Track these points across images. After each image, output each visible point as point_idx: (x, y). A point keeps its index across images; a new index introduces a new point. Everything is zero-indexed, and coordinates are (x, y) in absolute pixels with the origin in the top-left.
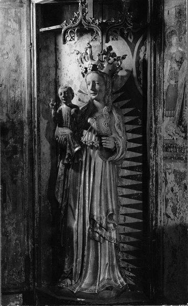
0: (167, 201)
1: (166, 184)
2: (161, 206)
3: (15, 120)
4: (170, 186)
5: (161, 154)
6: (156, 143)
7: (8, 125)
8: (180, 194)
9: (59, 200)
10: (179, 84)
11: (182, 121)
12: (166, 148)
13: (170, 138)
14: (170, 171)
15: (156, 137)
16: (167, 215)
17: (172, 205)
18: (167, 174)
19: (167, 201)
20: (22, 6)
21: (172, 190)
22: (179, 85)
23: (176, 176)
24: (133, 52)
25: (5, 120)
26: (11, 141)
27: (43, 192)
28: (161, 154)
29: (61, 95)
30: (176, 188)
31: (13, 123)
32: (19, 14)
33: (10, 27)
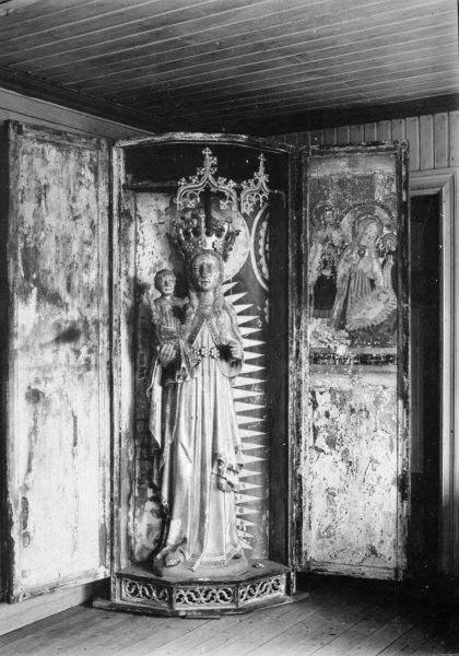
0: (316, 431)
1: (314, 408)
2: (307, 438)
3: (89, 319)
4: (321, 409)
5: (306, 366)
6: (298, 351)
7: (80, 326)
8: (342, 419)
9: (158, 438)
10: (339, 276)
11: (345, 323)
12: (315, 358)
13: (323, 346)
14: (322, 390)
15: (298, 344)
16: (316, 448)
17: (327, 434)
18: (317, 394)
19: (316, 431)
20: (99, 148)
21: (327, 415)
22: (338, 277)
23: (333, 396)
24: (250, 227)
25: (76, 319)
26: (84, 350)
27: (124, 428)
28: (306, 366)
29: (342, 281)
30: (334, 412)
31: (86, 322)
32: (95, 160)
33: (83, 176)
